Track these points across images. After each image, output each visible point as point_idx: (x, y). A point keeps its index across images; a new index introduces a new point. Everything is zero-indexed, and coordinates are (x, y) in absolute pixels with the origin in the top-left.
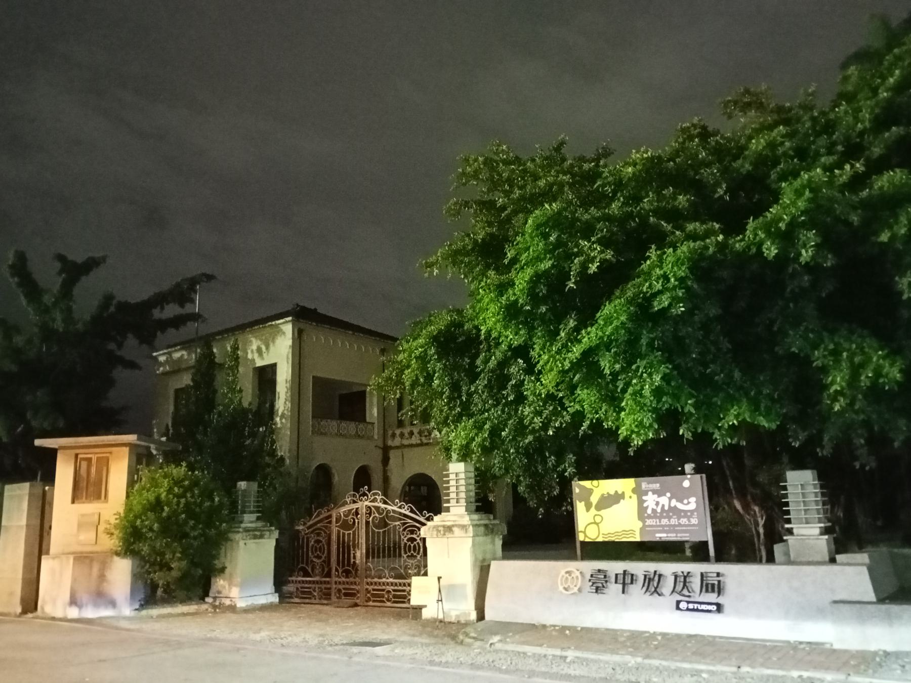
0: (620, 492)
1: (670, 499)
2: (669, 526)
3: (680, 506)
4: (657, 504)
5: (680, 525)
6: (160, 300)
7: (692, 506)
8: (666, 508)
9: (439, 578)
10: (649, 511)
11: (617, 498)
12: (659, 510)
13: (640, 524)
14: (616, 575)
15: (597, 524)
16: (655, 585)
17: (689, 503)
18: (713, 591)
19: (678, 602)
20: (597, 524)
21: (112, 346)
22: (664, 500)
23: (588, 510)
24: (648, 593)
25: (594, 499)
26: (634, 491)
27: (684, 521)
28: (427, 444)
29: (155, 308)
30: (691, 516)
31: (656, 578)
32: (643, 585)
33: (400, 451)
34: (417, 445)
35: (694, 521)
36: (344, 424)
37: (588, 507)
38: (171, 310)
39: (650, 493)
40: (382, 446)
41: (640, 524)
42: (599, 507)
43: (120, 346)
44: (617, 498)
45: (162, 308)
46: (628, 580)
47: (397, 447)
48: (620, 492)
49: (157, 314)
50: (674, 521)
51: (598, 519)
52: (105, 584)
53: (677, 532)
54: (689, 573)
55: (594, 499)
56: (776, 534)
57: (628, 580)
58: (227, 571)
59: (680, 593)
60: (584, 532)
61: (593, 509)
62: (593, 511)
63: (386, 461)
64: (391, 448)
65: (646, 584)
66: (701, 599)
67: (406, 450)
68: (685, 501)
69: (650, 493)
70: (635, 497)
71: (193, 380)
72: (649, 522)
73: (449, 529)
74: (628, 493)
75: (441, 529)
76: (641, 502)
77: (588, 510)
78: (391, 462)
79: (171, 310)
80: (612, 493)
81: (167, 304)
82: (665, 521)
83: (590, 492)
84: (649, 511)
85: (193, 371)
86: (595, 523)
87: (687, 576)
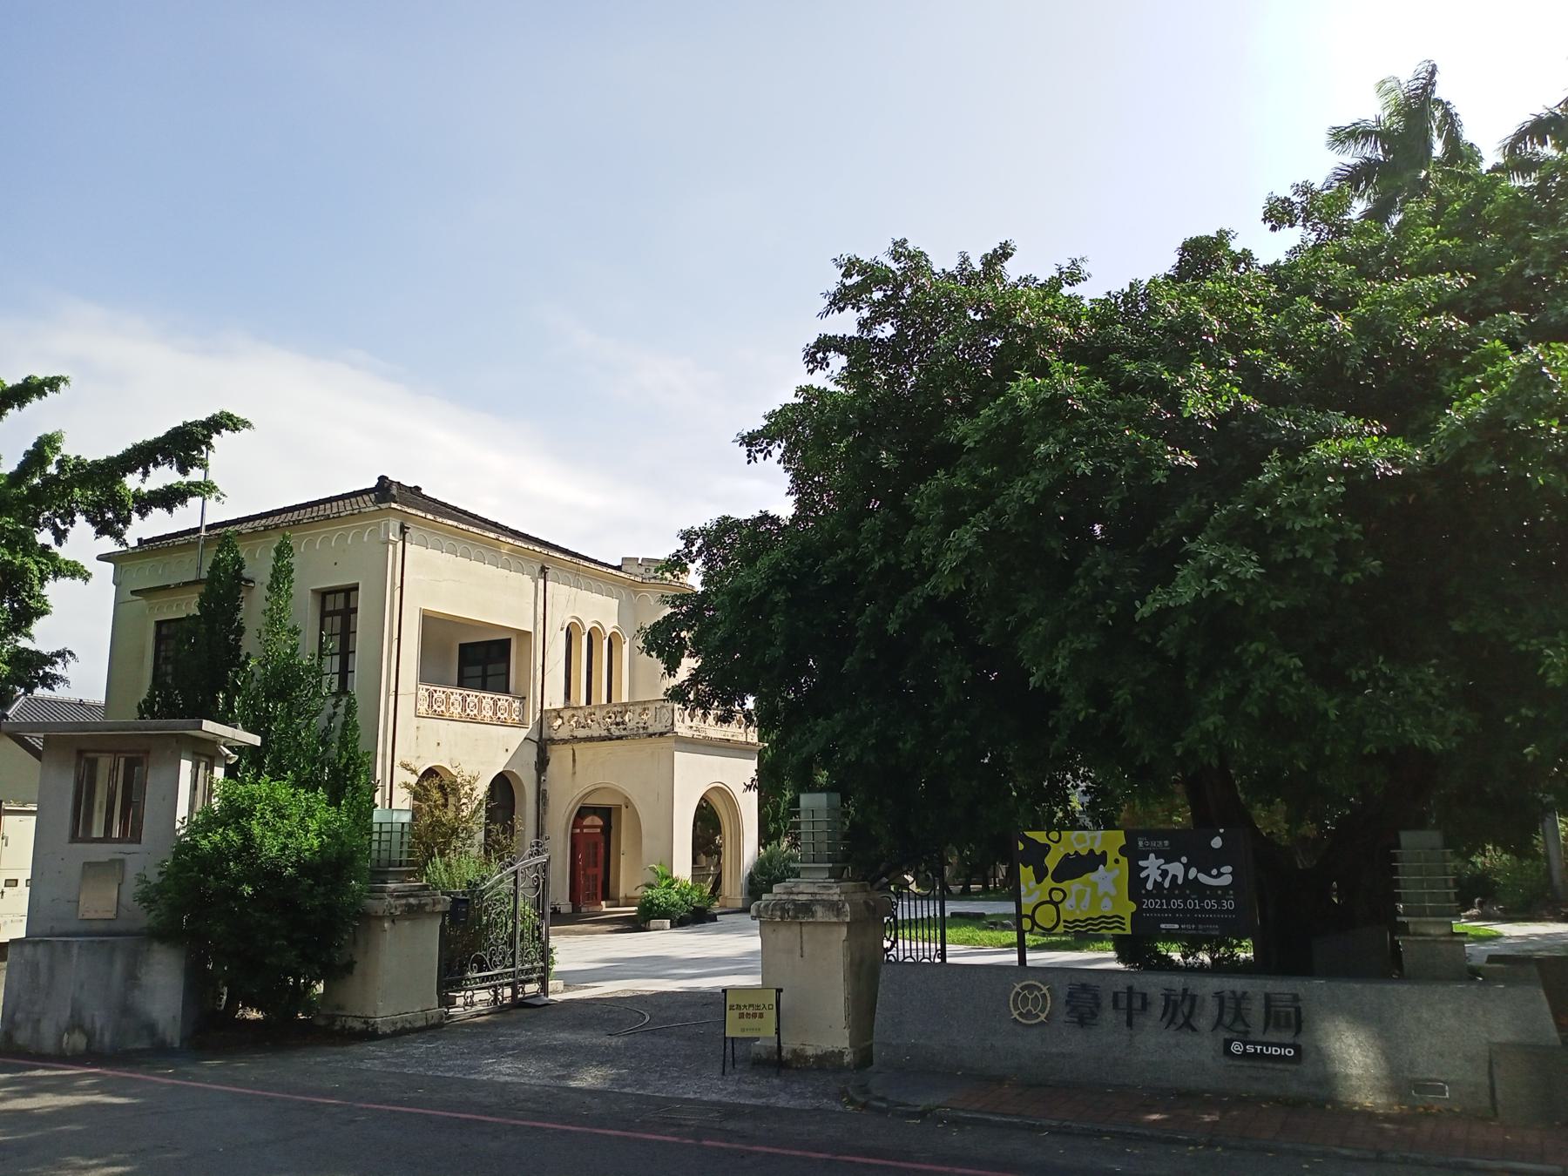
0: (1098, 852)
1: (1187, 868)
2: (1185, 911)
3: (1203, 878)
4: (1164, 874)
5: (1203, 910)
6: (142, 456)
7: (1226, 880)
8: (1180, 881)
9: (779, 991)
10: (1149, 886)
11: (1093, 861)
12: (1167, 884)
13: (1133, 907)
14: (1116, 994)
15: (1056, 904)
16: (1186, 1010)
17: (1220, 874)
18: (1288, 1026)
19: (1228, 1043)
20: (1056, 904)
21: (44, 537)
22: (1176, 869)
23: (1039, 881)
24: (1173, 1027)
25: (1051, 862)
26: (1122, 851)
27: (1211, 904)
28: (620, 738)
29: (133, 471)
30: (1223, 897)
31: (1187, 1005)
32: (1164, 1015)
33: (568, 747)
34: (602, 739)
35: (1228, 904)
36: (473, 696)
37: (1040, 875)
38: (164, 476)
39: (1152, 856)
40: (536, 738)
41: (1133, 907)
42: (1059, 876)
43: (60, 536)
44: (1093, 861)
45: (146, 473)
46: (1137, 1004)
47: (565, 741)
48: (1098, 852)
49: (132, 482)
50: (1194, 904)
51: (1057, 896)
52: (137, 993)
53: (1198, 921)
54: (1245, 993)
55: (1051, 862)
56: (583, 812)
57: (1137, 1004)
58: (358, 969)
59: (1229, 1029)
60: (1032, 917)
61: (1048, 879)
62: (1048, 882)
63: (542, 764)
64: (553, 741)
65: (1169, 1015)
66: (1265, 1039)
67: (577, 747)
68: (1214, 872)
69: (1152, 856)
70: (1124, 861)
71: (200, 606)
72: (1148, 903)
73: (806, 908)
74: (1113, 854)
75: (790, 906)
76: (1135, 870)
77: (1039, 881)
78: (549, 768)
79: (164, 476)
80: (1084, 853)
81: (156, 465)
82: (1177, 903)
83: (1045, 849)
84: (1149, 886)
85: (202, 588)
86: (1051, 901)
87: (1240, 999)
